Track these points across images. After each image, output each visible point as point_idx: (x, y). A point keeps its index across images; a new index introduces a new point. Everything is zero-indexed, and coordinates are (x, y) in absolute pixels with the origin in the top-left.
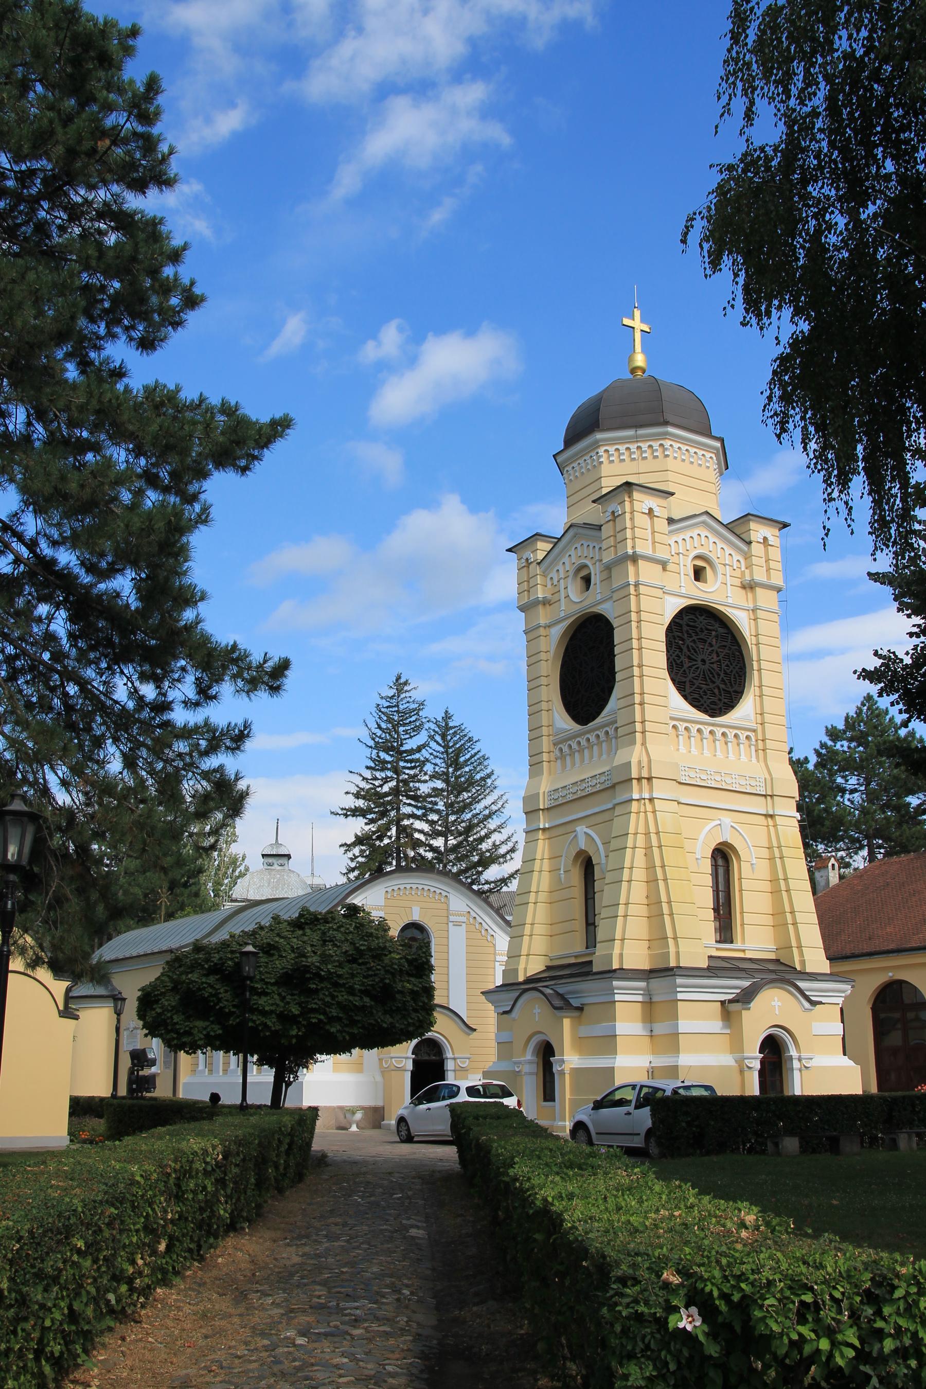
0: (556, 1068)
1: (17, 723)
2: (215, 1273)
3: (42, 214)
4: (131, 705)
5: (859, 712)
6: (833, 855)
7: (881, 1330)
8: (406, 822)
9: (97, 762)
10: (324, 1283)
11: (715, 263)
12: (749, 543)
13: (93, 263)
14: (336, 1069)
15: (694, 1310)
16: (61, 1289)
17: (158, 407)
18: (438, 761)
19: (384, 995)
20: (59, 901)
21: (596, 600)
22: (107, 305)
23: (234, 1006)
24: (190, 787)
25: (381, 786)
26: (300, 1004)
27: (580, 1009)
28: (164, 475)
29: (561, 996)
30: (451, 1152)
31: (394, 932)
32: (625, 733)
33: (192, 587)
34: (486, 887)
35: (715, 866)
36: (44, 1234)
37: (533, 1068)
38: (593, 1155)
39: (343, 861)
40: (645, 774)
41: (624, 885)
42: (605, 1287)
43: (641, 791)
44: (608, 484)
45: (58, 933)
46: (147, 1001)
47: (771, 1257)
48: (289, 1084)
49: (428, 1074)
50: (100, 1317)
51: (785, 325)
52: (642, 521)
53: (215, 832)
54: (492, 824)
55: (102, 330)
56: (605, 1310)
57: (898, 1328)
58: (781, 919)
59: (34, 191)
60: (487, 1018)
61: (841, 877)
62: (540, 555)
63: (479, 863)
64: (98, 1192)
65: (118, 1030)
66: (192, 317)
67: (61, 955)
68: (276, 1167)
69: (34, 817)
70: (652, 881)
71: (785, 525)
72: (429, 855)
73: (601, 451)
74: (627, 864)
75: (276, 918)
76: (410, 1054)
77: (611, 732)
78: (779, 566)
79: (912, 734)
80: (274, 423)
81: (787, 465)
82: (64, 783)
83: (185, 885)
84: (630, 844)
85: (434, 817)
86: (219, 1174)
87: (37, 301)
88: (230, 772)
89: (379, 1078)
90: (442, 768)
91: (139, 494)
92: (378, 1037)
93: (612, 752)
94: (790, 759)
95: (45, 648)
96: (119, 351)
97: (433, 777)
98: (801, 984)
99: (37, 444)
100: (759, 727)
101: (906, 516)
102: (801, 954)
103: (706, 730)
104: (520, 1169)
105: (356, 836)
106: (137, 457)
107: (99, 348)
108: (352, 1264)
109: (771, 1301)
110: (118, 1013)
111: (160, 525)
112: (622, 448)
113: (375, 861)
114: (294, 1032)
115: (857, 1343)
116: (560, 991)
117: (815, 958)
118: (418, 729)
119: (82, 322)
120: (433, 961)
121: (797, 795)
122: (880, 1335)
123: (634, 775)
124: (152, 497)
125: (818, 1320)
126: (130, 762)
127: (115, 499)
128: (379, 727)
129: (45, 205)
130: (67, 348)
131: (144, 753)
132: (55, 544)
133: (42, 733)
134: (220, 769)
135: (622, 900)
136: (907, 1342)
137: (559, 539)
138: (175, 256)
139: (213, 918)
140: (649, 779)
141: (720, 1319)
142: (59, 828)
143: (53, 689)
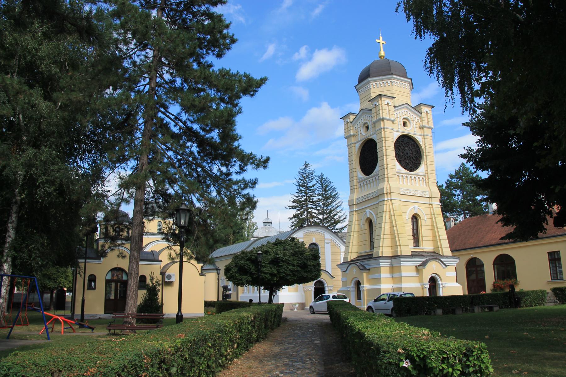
0: (361, 289)
1: (182, 181)
2: (252, 354)
3: (184, 16)
4: (218, 174)
5: (460, 169)
6: (452, 217)
7: (469, 365)
8: (310, 210)
9: (208, 193)
10: (288, 358)
11: (408, 19)
13: (201, 30)
14: (289, 291)
15: (408, 361)
16: (205, 358)
17: (223, 76)
19: (304, 266)
20: (198, 238)
22: (206, 44)
24: (239, 200)
26: (277, 270)
28: (226, 98)
29: (363, 266)
30: (328, 316)
31: (307, 246)
32: (382, 178)
33: (237, 134)
34: (337, 231)
35: (413, 221)
36: (198, 341)
37: (354, 289)
38: (374, 315)
39: (290, 223)
41: (383, 228)
42: (379, 354)
43: (387, 197)
44: (373, 95)
45: (198, 249)
46: (227, 270)
47: (433, 344)
48: (274, 296)
49: (319, 292)
50: (217, 367)
51: (430, 39)
52: (385, 107)
53: (247, 214)
54: (338, 210)
55: (205, 52)
56: (379, 361)
57: (474, 364)
58: (435, 239)
59: (181, 8)
60: (338, 273)
61: (455, 224)
62: (351, 120)
63: (334, 223)
64: (214, 329)
65: (218, 279)
66: (233, 46)
67: (199, 256)
68: (271, 322)
69: (189, 211)
70: (392, 227)
71: (433, 107)
72: (318, 221)
73: (371, 84)
74: (383, 222)
75: (268, 242)
76: (313, 286)
77: (377, 178)
78: (432, 121)
79: (477, 176)
80: (262, 80)
81: (433, 87)
82: (198, 200)
83: (238, 233)
84: (384, 215)
85: (319, 208)
86: (252, 324)
87: (183, 43)
88: (251, 195)
89: (303, 294)
91: (218, 105)
92: (302, 280)
93: (377, 185)
94: (437, 186)
95: (190, 157)
96: (210, 58)
97: (318, 195)
98: (442, 259)
99: (185, 90)
101: (472, 101)
102: (442, 249)
103: (409, 176)
104: (350, 320)
106: (217, 93)
107: (203, 58)
108: (297, 352)
109: (433, 357)
110: (218, 274)
111: (226, 114)
112: (378, 83)
113: (300, 223)
114: (275, 279)
115: (461, 369)
116: (362, 264)
117: (446, 250)
118: (312, 179)
119: (198, 50)
120: (320, 255)
121: (439, 197)
122: (468, 366)
124: (223, 105)
125: (448, 363)
126: (219, 193)
127: (211, 107)
129: (185, 13)
130: (194, 58)
131: (223, 189)
132: (192, 122)
133: (190, 184)
134: (248, 194)
135: (382, 234)
136: (477, 368)
138: (227, 27)
139: (248, 243)
140: (390, 193)
141: (417, 363)
142: (197, 215)
143: (193, 170)
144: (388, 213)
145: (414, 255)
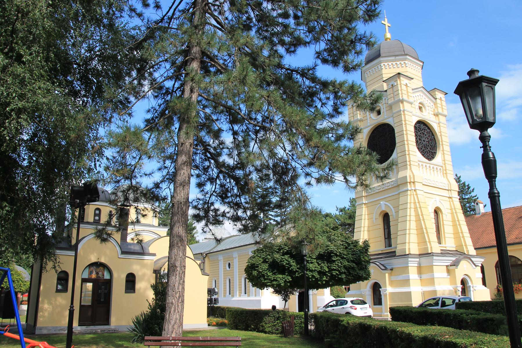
12: (436, 99)
21: (385, 118)
23: (298, 268)
26: (328, 267)
27: (392, 270)
40: (412, 181)
41: (408, 222)
43: (411, 186)
52: (404, 87)
58: (457, 235)
73: (382, 64)
74: (408, 214)
84: (409, 207)
98: (473, 259)
100: (444, 165)
102: (467, 248)
103: (428, 165)
112: (390, 64)
114: (325, 278)
121: (458, 190)
123: (408, 181)
135: (408, 228)
144: (412, 204)
145: (445, 253)
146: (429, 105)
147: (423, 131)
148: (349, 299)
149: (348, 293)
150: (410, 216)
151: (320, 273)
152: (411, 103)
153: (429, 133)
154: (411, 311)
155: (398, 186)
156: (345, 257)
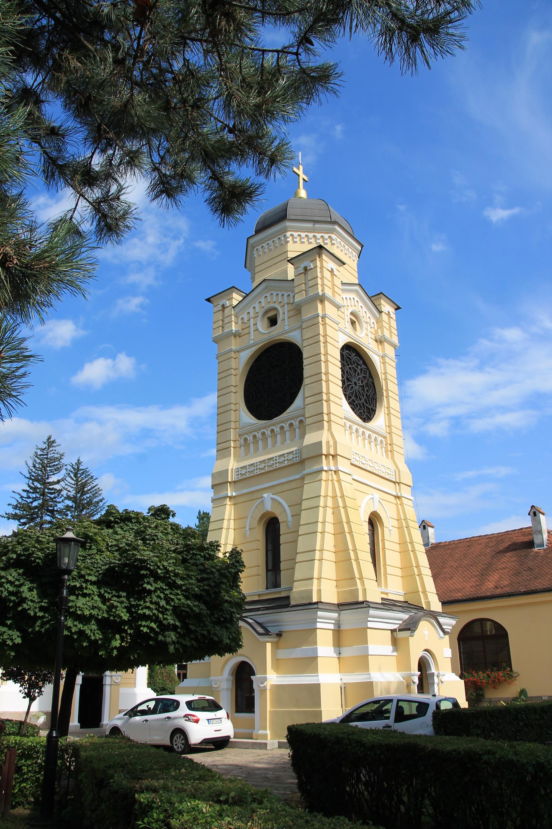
18: (70, 489)
21: (286, 331)
23: (41, 609)
25: (32, 503)
26: (129, 609)
27: (279, 635)
40: (332, 452)
41: (319, 535)
43: (328, 463)
52: (327, 274)
58: (409, 572)
62: (235, 303)
73: (288, 234)
74: (320, 519)
84: (322, 504)
90: (72, 493)
103: (361, 430)
105: (14, 532)
112: (303, 235)
114: (116, 643)
116: (260, 620)
118: (58, 470)
123: (324, 452)
128: (34, 466)
137: (247, 295)
144: (330, 500)
146: (368, 320)
147: (354, 366)
148: (183, 699)
149: (182, 684)
150: (324, 522)
151: (103, 624)
152: (338, 307)
153: (365, 373)
154: (360, 744)
155: (302, 462)
156: (180, 582)
